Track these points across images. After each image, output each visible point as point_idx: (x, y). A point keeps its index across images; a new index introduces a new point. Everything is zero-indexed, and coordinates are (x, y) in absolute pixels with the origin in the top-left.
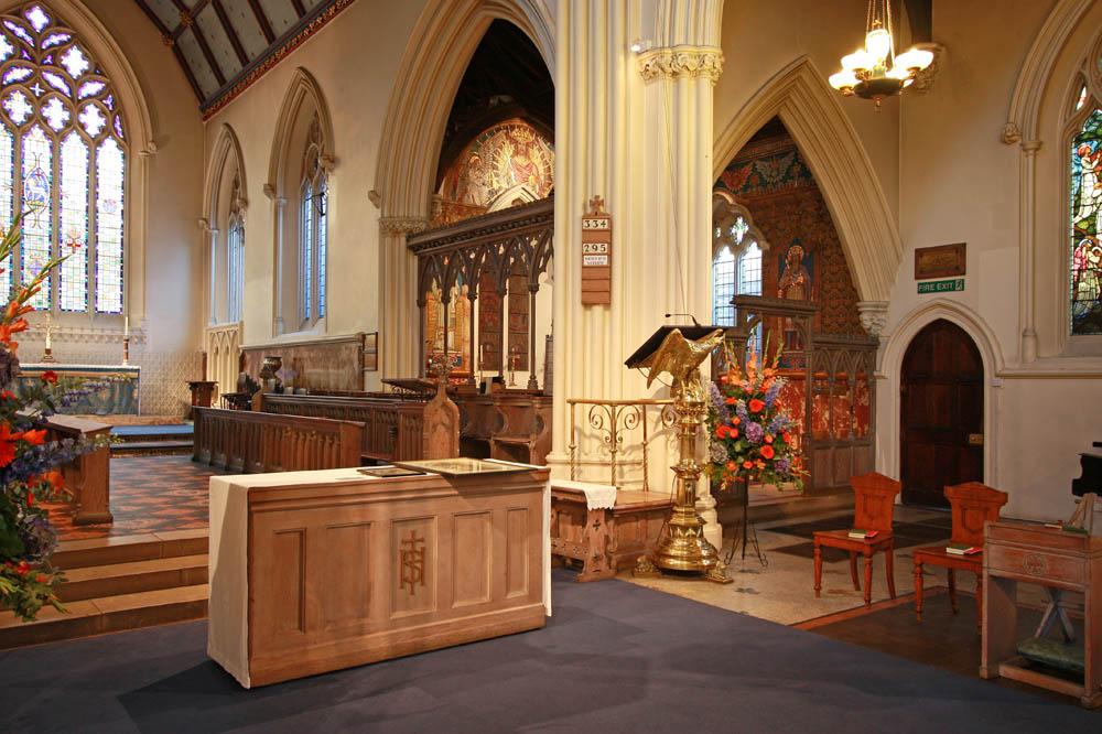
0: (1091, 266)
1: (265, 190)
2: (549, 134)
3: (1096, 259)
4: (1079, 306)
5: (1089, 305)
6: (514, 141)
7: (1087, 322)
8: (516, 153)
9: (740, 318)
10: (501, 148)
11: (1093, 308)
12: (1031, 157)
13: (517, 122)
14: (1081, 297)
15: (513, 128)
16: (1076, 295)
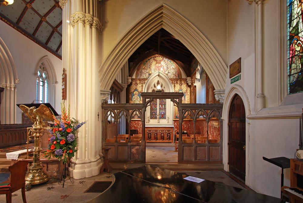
0: (296, 53)
1: (57, 83)
2: (61, 59)
3: (298, 49)
4: (292, 77)
5: (296, 76)
6: (155, 60)
7: (295, 87)
8: (157, 63)
9: (144, 101)
10: (152, 63)
11: (298, 77)
12: (260, 6)
13: (157, 55)
14: (293, 72)
15: (156, 57)
16: (290, 72)
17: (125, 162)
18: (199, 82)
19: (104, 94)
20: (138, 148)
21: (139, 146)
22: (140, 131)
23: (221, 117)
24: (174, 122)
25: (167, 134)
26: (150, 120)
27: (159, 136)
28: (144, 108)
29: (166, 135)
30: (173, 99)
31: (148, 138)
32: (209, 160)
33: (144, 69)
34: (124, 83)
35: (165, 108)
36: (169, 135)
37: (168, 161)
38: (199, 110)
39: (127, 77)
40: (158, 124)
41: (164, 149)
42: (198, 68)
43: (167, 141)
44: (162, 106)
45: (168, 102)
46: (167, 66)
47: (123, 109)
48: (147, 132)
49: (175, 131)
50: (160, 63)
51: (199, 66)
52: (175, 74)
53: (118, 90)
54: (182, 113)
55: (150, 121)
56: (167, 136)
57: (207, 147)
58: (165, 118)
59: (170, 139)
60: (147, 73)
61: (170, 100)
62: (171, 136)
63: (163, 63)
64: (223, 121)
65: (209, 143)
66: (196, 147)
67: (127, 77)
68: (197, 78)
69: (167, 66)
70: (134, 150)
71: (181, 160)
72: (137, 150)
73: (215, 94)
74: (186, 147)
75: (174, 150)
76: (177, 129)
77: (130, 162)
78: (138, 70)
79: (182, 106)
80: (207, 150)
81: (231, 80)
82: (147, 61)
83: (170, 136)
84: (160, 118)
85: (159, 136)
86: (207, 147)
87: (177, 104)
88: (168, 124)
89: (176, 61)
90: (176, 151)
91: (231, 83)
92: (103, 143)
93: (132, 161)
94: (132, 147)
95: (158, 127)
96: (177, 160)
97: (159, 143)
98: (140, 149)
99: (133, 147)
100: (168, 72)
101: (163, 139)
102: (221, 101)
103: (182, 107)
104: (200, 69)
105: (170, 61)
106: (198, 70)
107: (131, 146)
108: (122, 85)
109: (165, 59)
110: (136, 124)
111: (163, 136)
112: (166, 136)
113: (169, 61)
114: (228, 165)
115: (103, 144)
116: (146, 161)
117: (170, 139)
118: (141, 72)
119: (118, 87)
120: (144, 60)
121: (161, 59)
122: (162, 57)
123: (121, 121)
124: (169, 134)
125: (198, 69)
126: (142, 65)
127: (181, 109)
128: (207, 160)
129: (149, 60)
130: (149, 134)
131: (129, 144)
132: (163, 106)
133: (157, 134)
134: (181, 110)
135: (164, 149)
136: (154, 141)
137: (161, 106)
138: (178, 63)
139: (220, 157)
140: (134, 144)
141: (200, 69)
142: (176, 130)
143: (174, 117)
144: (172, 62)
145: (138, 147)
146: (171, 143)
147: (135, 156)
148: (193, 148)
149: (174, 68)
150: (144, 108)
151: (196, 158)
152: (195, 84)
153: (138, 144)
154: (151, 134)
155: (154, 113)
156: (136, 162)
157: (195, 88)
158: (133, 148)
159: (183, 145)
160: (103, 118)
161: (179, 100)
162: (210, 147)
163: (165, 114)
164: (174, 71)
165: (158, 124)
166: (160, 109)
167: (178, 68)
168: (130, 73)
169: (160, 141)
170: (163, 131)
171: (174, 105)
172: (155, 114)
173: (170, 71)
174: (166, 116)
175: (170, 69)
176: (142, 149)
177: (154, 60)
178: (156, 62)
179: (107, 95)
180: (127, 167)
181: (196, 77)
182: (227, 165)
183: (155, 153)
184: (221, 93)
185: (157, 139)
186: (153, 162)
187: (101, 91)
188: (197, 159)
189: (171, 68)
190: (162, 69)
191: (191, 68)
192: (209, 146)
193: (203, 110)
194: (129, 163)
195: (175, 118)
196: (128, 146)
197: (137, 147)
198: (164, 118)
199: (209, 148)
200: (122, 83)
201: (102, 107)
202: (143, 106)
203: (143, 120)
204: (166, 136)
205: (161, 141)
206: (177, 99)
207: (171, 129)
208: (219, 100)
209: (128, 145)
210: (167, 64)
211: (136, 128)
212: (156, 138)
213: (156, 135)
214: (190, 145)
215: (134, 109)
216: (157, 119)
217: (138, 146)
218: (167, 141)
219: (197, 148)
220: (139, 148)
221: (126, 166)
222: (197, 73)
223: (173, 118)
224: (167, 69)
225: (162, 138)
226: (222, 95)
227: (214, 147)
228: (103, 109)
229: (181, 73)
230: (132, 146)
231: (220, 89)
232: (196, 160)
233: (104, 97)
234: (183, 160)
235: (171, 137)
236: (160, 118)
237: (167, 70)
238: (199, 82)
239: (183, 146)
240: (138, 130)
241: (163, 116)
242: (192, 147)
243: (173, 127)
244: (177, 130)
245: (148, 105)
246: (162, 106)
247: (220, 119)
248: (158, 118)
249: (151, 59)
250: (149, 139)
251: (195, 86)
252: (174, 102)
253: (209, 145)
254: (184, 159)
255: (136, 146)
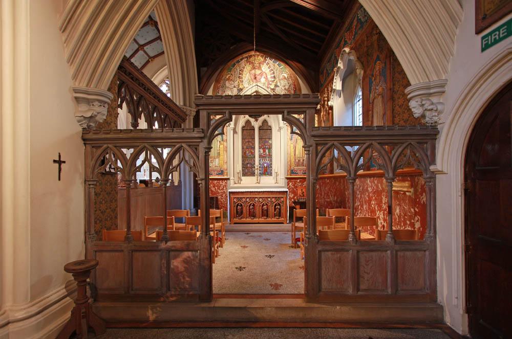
8: (254, 68)
10: (244, 68)
13: (253, 53)
15: (251, 56)
17: (152, 298)
18: (340, 97)
19: (88, 102)
20: (189, 257)
21: (192, 251)
22: (222, 199)
23: (433, 161)
24: (287, 181)
25: (275, 206)
26: (243, 178)
27: (258, 211)
28: (206, 141)
29: (273, 208)
30: (289, 113)
31: (237, 214)
32: (397, 290)
33: (228, 79)
34: (190, 107)
35: (270, 156)
36: (279, 207)
37: (277, 286)
38: (365, 146)
39: (196, 94)
40: (258, 185)
41: (267, 240)
42: (339, 65)
43: (274, 220)
44: (264, 151)
45: (276, 122)
46: (274, 73)
47: (146, 145)
48: (234, 202)
49: (290, 199)
50: (259, 68)
51: (342, 59)
52: (289, 88)
53: (176, 118)
54: (314, 155)
55: (241, 180)
56: (275, 209)
57: (389, 252)
58: (271, 174)
59: (280, 215)
60: (235, 87)
61: (280, 116)
62: (283, 208)
63: (265, 68)
64: (435, 178)
65: (395, 242)
66: (358, 252)
67: (196, 94)
68: (335, 90)
69: (274, 73)
70: (177, 263)
71: (314, 292)
72: (186, 261)
73: (411, 98)
74: (329, 253)
75: (290, 242)
76: (293, 195)
77: (167, 297)
78: (218, 81)
79: (315, 133)
80: (389, 261)
81: (483, 38)
82: (235, 64)
83: (280, 209)
84: (260, 173)
85: (258, 211)
86: (389, 252)
87: (300, 129)
88: (277, 185)
89: (290, 62)
90: (295, 246)
91: (483, 50)
92: (89, 245)
93: (172, 296)
94: (172, 253)
95: (257, 192)
96: (299, 283)
97: (258, 223)
98: (194, 260)
99: (176, 253)
100: (276, 86)
101: (267, 216)
102: (429, 118)
103: (314, 136)
104: (342, 68)
105: (278, 65)
106: (337, 71)
107: (169, 250)
108: (185, 110)
109: (268, 59)
110: (214, 187)
111: (267, 210)
112: (271, 210)
113: (276, 65)
114: (467, 315)
115: (89, 245)
116: (215, 290)
117: (280, 215)
118: (224, 86)
119: (177, 114)
120: (229, 64)
121: (262, 59)
122: (262, 56)
123: (182, 181)
124: (279, 205)
125: (339, 68)
126: (225, 72)
127: (312, 141)
128: (389, 291)
129: (238, 62)
130: (238, 205)
131: (163, 245)
132: (267, 151)
133: (254, 205)
134: (311, 146)
135: (267, 240)
136: (249, 220)
137: (262, 151)
138: (294, 65)
139: (428, 283)
140: (178, 244)
141: (342, 68)
142: (292, 196)
143: (288, 171)
144: (283, 65)
145: (190, 254)
146: (283, 223)
147: (182, 280)
148: (350, 255)
149: (286, 77)
150: (206, 141)
151: (358, 284)
152: (330, 103)
153: (188, 245)
154: (241, 205)
155: (249, 165)
156: (185, 298)
157: (330, 111)
158: (175, 257)
159: (320, 248)
160: (90, 170)
161: (305, 118)
162: (399, 253)
163: (270, 166)
164: (286, 82)
165: (258, 185)
166: (260, 156)
167: (294, 77)
168: (202, 85)
169: (260, 219)
170: (266, 199)
171: (292, 132)
172: (252, 168)
173: (279, 84)
174: (273, 170)
175: (279, 80)
176: (200, 260)
177: (248, 61)
178: (251, 66)
179: (96, 103)
180: (154, 316)
181: (334, 88)
182: (463, 316)
183: (246, 251)
184: (430, 94)
185: (254, 217)
186: (235, 291)
187: (76, 91)
188: (362, 287)
189: (281, 77)
190: (263, 80)
191: (321, 76)
192: (397, 251)
193: (378, 146)
194: (164, 301)
195: (289, 173)
196: (160, 251)
197: (187, 254)
198: (268, 174)
199: (396, 255)
200: (185, 104)
201: (84, 140)
202: (202, 135)
203: (204, 177)
204: (271, 210)
205: (262, 220)
206: (299, 113)
207: (282, 196)
208: (423, 116)
209: (160, 248)
210: (272, 70)
211: (215, 193)
212: (253, 215)
213: (251, 207)
214: (339, 247)
215: (178, 146)
216: (256, 177)
217: (188, 250)
218: (274, 220)
219: (360, 254)
220: (193, 256)
221: (153, 313)
222: (335, 77)
223: (285, 174)
224: (273, 79)
225: (265, 214)
226: (434, 99)
227: (408, 254)
228: (89, 147)
229: (300, 85)
230: (173, 251)
231: (428, 81)
232: (358, 290)
233: (89, 110)
234: (320, 290)
235: (283, 211)
236: (261, 174)
237: (273, 81)
238: (340, 97)
239: (320, 252)
240: (219, 197)
241: (266, 171)
242: (345, 253)
243: (287, 192)
244: (294, 197)
245: (217, 132)
246: (264, 151)
247: (427, 170)
248: (256, 173)
249: (242, 60)
250: (239, 216)
251: (331, 108)
252: (291, 122)
253: (397, 247)
254: (323, 287)
255: (182, 250)
